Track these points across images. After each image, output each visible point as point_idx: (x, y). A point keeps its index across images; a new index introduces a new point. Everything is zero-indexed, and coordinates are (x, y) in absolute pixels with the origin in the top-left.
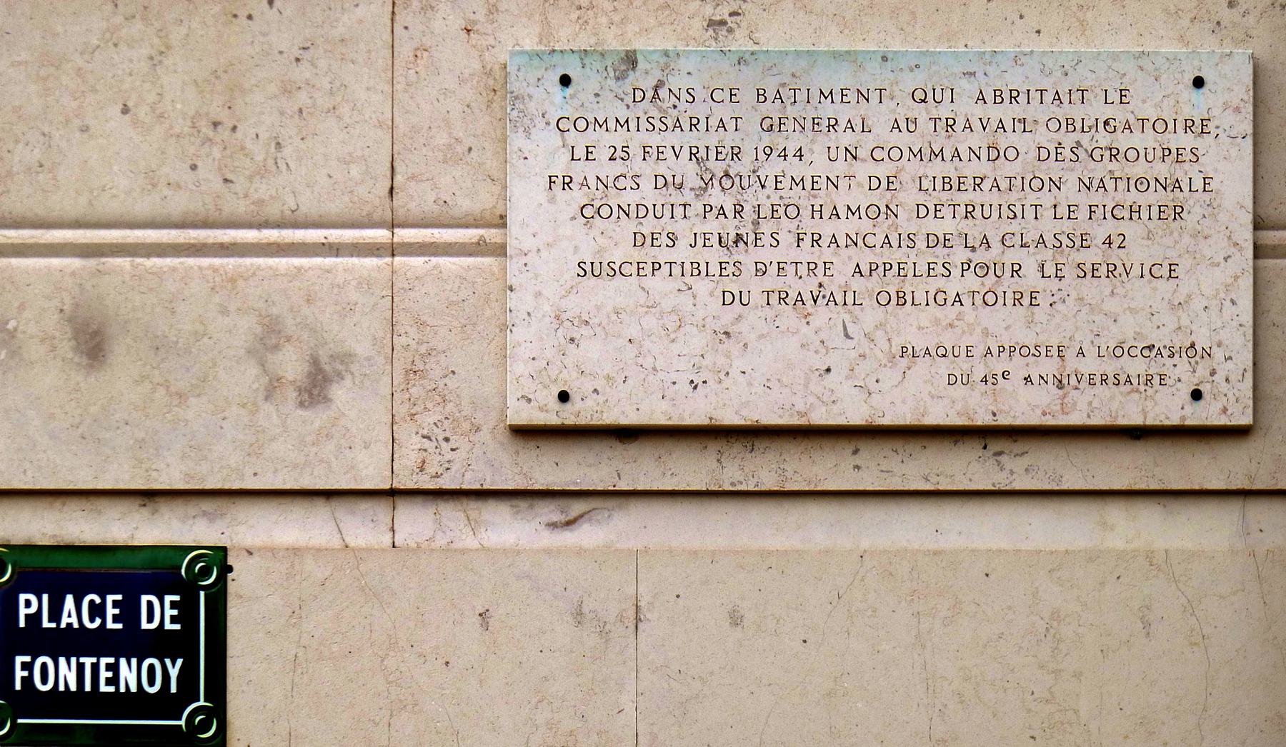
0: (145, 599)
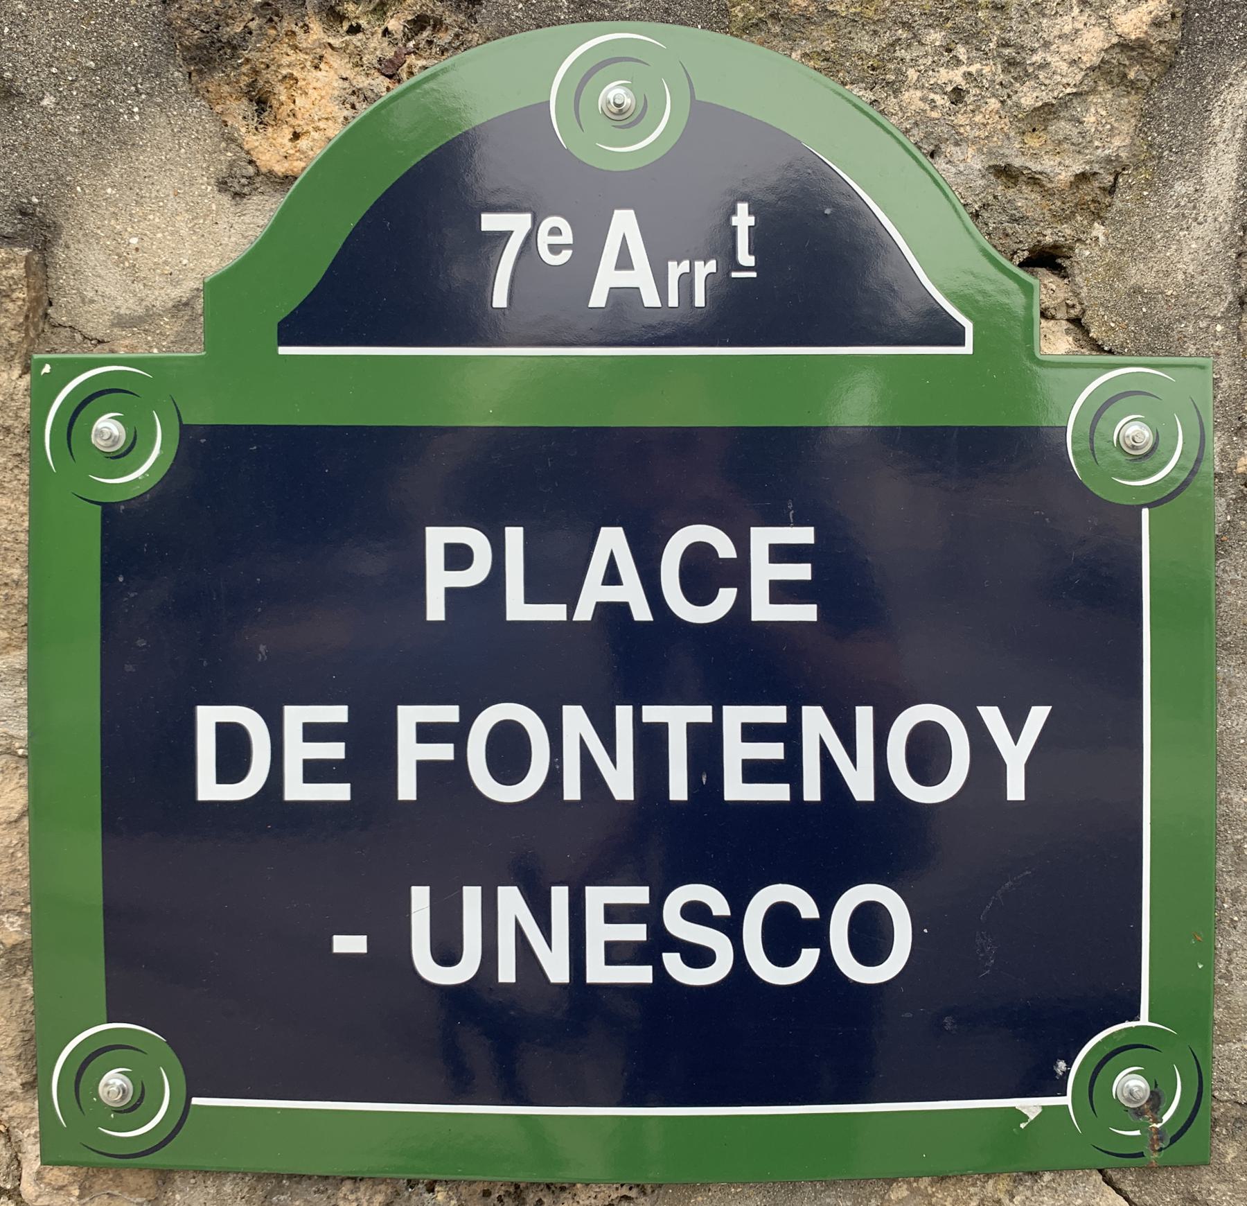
0: (208, 718)
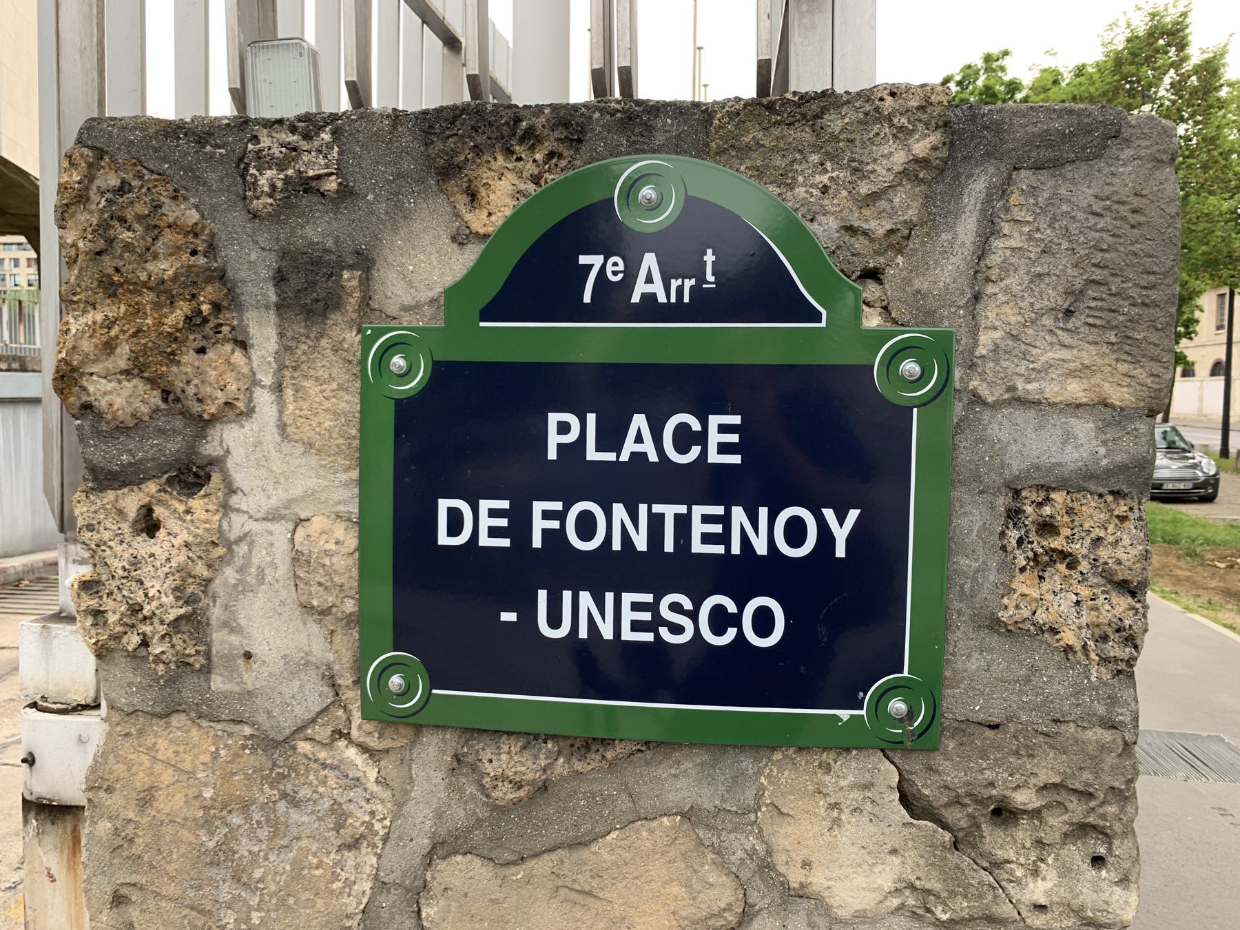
0: (444, 505)
